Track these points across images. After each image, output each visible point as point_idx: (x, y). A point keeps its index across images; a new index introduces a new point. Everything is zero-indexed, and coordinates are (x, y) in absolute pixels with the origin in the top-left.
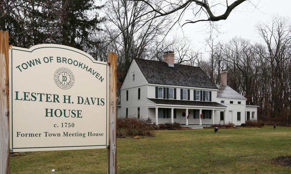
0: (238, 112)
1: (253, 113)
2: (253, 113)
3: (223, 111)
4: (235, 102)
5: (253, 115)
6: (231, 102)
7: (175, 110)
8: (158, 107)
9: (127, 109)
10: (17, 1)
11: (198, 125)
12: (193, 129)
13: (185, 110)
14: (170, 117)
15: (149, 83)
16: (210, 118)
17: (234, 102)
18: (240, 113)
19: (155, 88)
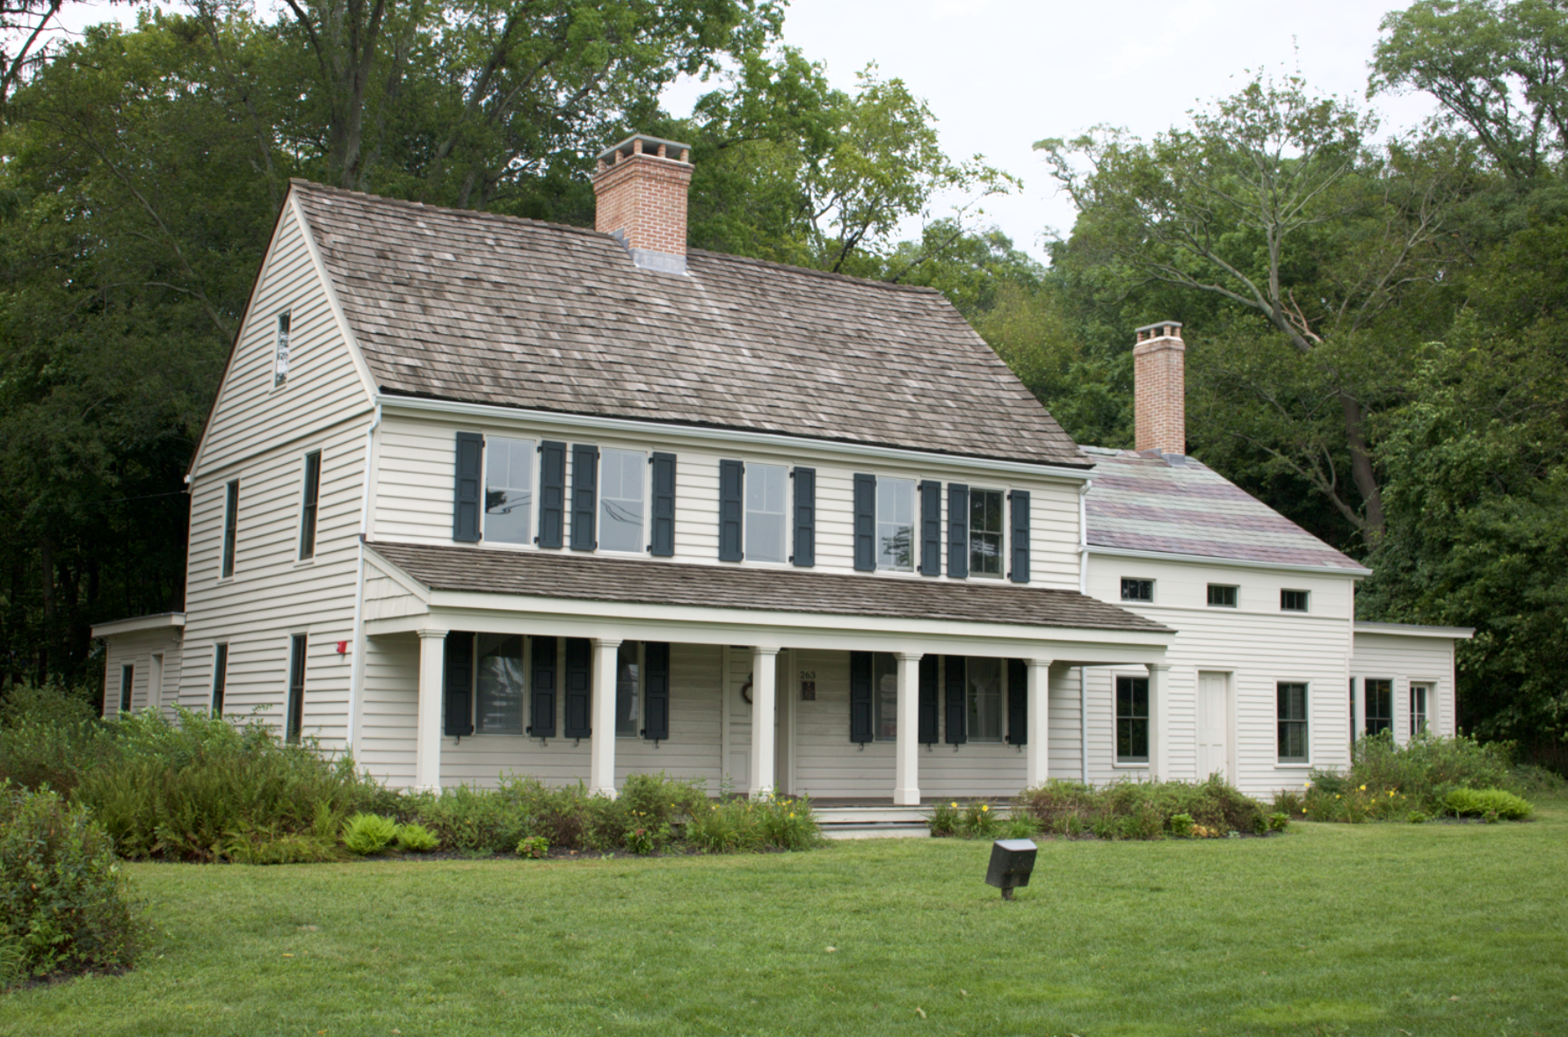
0: (1283, 688)
1: (1421, 693)
2: (1419, 693)
3: (1139, 671)
4: (1259, 594)
5: (1421, 708)
6: (1222, 596)
8: (617, 635)
9: (300, 643)
11: (887, 802)
16: (1019, 735)
17: (1242, 596)
18: (1301, 688)
19: (452, 446)
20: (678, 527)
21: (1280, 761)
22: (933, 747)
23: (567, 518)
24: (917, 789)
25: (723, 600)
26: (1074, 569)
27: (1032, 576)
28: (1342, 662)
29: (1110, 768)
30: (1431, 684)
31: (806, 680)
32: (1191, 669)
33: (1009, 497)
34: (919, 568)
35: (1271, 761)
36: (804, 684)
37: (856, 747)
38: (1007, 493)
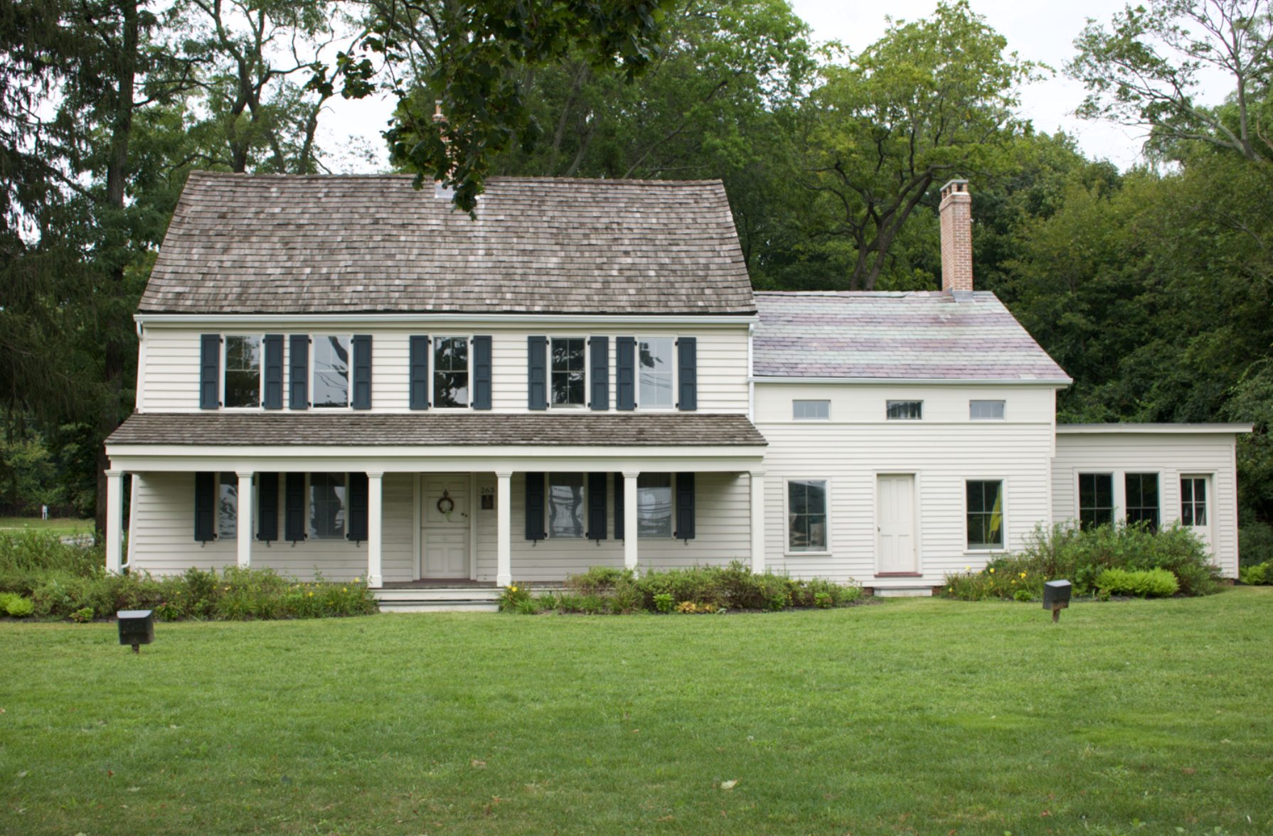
1: (1200, 484)
2: (1194, 488)
7: (265, 482)
10: (9, 127)
12: (909, 599)
13: (491, 478)
14: (232, 535)
15: (743, 416)
17: (925, 409)
20: (699, 388)
21: (969, 548)
22: (602, 542)
23: (286, 387)
24: (509, 575)
25: (357, 439)
26: (744, 397)
27: (699, 404)
28: (1043, 461)
29: (782, 556)
30: (1210, 475)
31: (485, 494)
32: (870, 473)
33: (589, 343)
34: (589, 405)
35: (960, 548)
36: (484, 498)
37: (531, 543)
38: (588, 339)
